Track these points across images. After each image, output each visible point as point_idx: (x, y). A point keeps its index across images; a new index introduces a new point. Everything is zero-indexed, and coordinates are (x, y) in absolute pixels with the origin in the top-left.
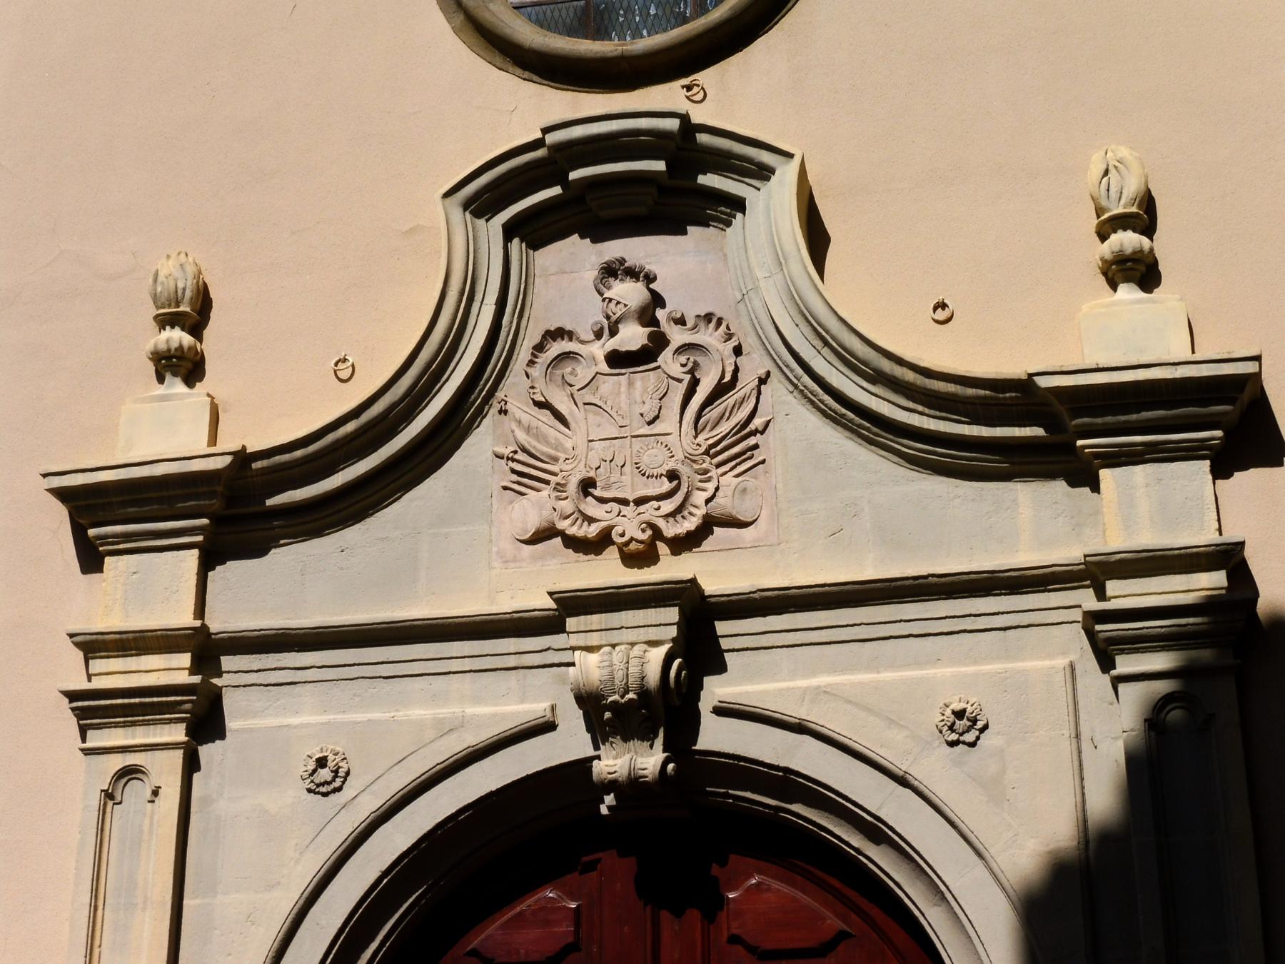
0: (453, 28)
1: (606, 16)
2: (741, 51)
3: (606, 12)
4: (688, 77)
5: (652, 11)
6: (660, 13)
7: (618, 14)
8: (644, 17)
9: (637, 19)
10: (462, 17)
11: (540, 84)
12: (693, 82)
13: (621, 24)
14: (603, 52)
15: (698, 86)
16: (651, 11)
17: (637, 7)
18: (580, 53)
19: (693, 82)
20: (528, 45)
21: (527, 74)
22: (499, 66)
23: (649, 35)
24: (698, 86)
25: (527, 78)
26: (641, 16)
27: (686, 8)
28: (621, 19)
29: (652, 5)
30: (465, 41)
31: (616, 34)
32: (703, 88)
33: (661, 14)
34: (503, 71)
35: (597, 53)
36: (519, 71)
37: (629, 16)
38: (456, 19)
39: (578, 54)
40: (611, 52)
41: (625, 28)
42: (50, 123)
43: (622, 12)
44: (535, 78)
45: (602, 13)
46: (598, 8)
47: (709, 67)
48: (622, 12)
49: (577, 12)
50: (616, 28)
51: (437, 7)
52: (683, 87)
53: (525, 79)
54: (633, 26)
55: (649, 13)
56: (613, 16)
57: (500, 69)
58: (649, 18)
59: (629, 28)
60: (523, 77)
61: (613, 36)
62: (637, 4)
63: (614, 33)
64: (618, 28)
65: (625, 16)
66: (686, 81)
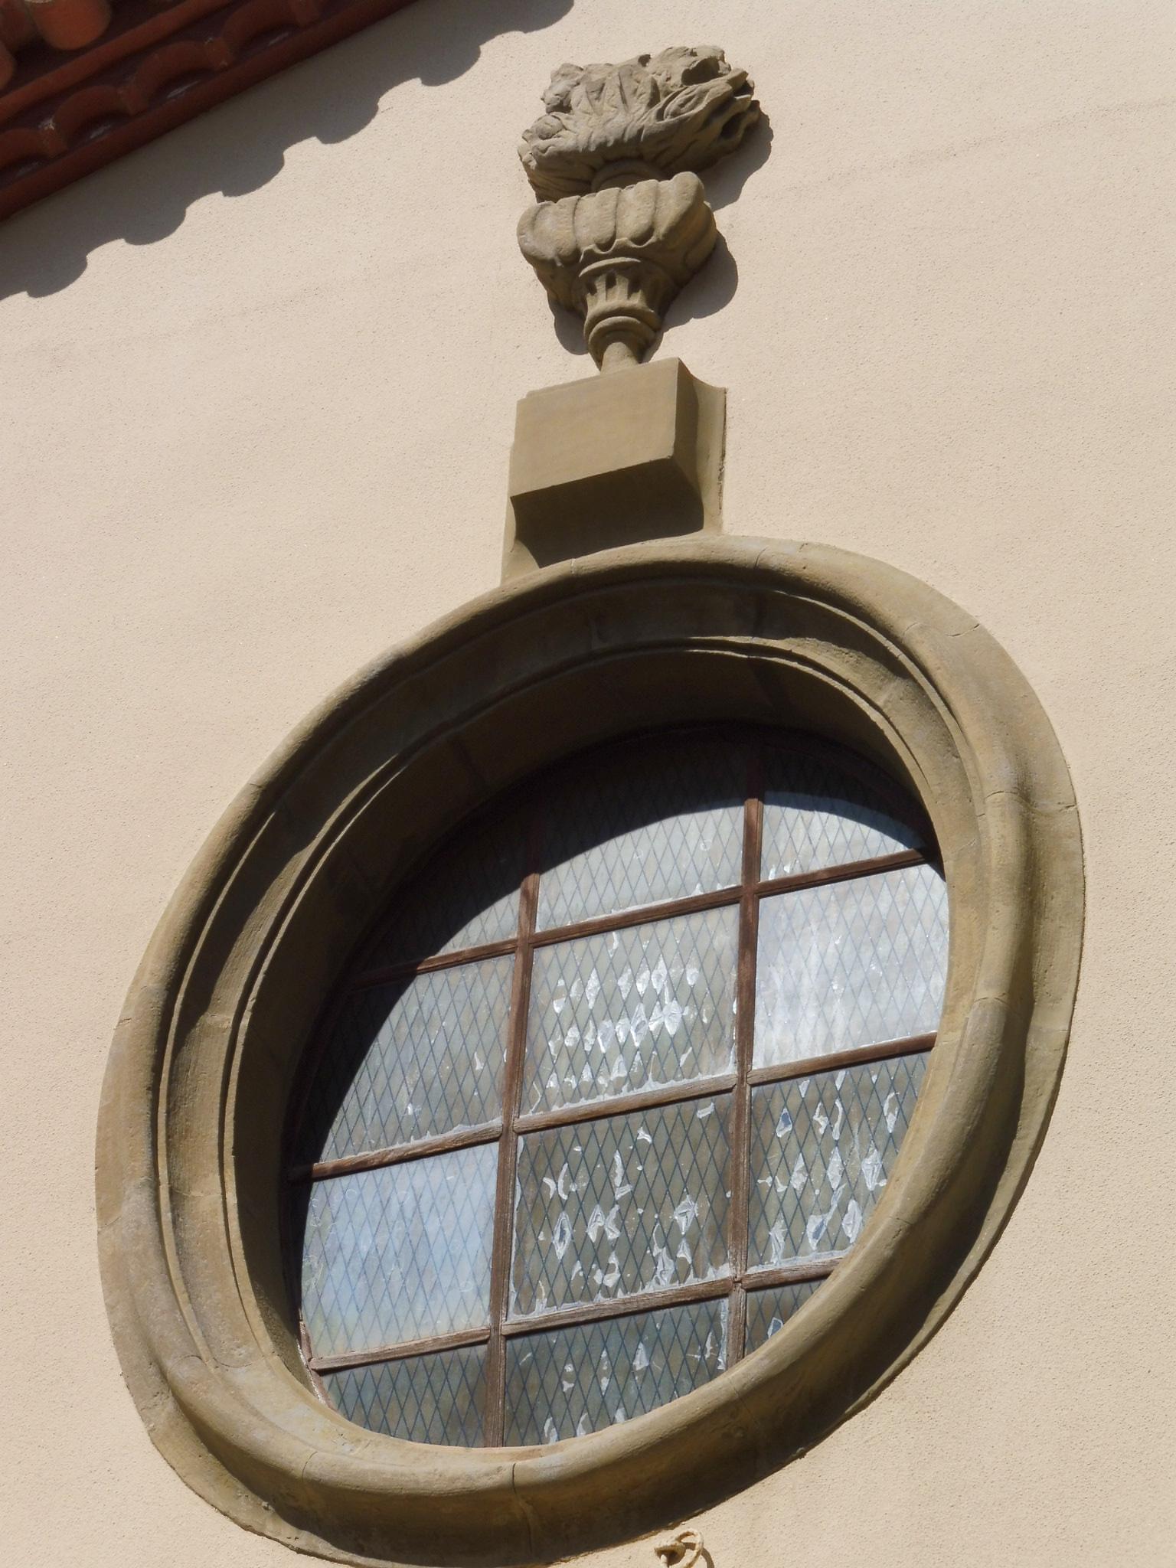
0: (150, 1431)
1: (533, 1380)
2: (802, 1455)
3: (534, 1372)
4: (672, 1528)
5: (640, 1362)
6: (658, 1367)
7: (561, 1376)
8: (621, 1379)
9: (605, 1383)
10: (170, 1405)
11: (332, 1560)
12: (685, 1540)
13: (568, 1399)
14: (470, 1477)
15: (691, 1546)
16: (636, 1363)
17: (604, 1354)
18: (417, 1482)
19: (685, 1540)
20: (301, 1467)
21: (306, 1539)
22: (246, 1520)
23: (628, 1417)
24: (691, 1546)
25: (306, 1548)
26: (613, 1375)
27: (717, 1350)
28: (567, 1386)
29: (641, 1346)
30: (174, 1464)
31: (554, 1423)
32: (706, 1554)
33: (661, 1369)
34: (254, 1532)
35: (453, 1480)
36: (287, 1531)
37: (587, 1377)
38: (158, 1409)
39: (412, 1485)
40: (487, 1474)
41: (575, 1408)
42: (850, 347)
43: (569, 1368)
44: (324, 1546)
45: (524, 1373)
46: (517, 1362)
47: (724, 1500)
48: (569, 1368)
49: (468, 1375)
50: (556, 1409)
51: (122, 1382)
52: (660, 1552)
53: (299, 1551)
54: (594, 1400)
55: (631, 1367)
56: (551, 1379)
57: (246, 1528)
58: (630, 1381)
59: (585, 1407)
60: (297, 1544)
61: (546, 1428)
62: (605, 1347)
63: (549, 1421)
64: (559, 1407)
65: (577, 1378)
66: (666, 1538)
